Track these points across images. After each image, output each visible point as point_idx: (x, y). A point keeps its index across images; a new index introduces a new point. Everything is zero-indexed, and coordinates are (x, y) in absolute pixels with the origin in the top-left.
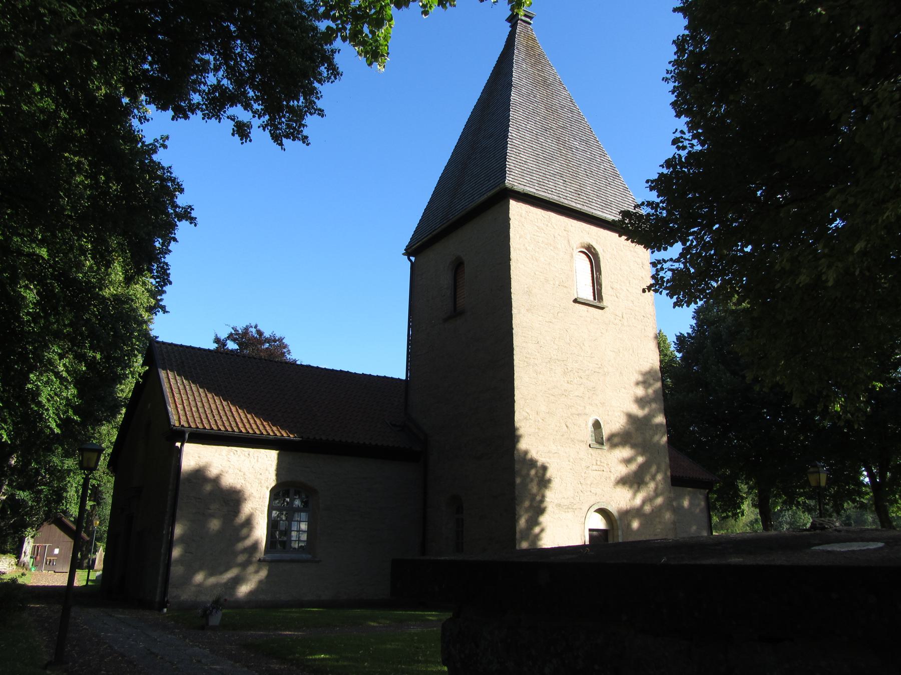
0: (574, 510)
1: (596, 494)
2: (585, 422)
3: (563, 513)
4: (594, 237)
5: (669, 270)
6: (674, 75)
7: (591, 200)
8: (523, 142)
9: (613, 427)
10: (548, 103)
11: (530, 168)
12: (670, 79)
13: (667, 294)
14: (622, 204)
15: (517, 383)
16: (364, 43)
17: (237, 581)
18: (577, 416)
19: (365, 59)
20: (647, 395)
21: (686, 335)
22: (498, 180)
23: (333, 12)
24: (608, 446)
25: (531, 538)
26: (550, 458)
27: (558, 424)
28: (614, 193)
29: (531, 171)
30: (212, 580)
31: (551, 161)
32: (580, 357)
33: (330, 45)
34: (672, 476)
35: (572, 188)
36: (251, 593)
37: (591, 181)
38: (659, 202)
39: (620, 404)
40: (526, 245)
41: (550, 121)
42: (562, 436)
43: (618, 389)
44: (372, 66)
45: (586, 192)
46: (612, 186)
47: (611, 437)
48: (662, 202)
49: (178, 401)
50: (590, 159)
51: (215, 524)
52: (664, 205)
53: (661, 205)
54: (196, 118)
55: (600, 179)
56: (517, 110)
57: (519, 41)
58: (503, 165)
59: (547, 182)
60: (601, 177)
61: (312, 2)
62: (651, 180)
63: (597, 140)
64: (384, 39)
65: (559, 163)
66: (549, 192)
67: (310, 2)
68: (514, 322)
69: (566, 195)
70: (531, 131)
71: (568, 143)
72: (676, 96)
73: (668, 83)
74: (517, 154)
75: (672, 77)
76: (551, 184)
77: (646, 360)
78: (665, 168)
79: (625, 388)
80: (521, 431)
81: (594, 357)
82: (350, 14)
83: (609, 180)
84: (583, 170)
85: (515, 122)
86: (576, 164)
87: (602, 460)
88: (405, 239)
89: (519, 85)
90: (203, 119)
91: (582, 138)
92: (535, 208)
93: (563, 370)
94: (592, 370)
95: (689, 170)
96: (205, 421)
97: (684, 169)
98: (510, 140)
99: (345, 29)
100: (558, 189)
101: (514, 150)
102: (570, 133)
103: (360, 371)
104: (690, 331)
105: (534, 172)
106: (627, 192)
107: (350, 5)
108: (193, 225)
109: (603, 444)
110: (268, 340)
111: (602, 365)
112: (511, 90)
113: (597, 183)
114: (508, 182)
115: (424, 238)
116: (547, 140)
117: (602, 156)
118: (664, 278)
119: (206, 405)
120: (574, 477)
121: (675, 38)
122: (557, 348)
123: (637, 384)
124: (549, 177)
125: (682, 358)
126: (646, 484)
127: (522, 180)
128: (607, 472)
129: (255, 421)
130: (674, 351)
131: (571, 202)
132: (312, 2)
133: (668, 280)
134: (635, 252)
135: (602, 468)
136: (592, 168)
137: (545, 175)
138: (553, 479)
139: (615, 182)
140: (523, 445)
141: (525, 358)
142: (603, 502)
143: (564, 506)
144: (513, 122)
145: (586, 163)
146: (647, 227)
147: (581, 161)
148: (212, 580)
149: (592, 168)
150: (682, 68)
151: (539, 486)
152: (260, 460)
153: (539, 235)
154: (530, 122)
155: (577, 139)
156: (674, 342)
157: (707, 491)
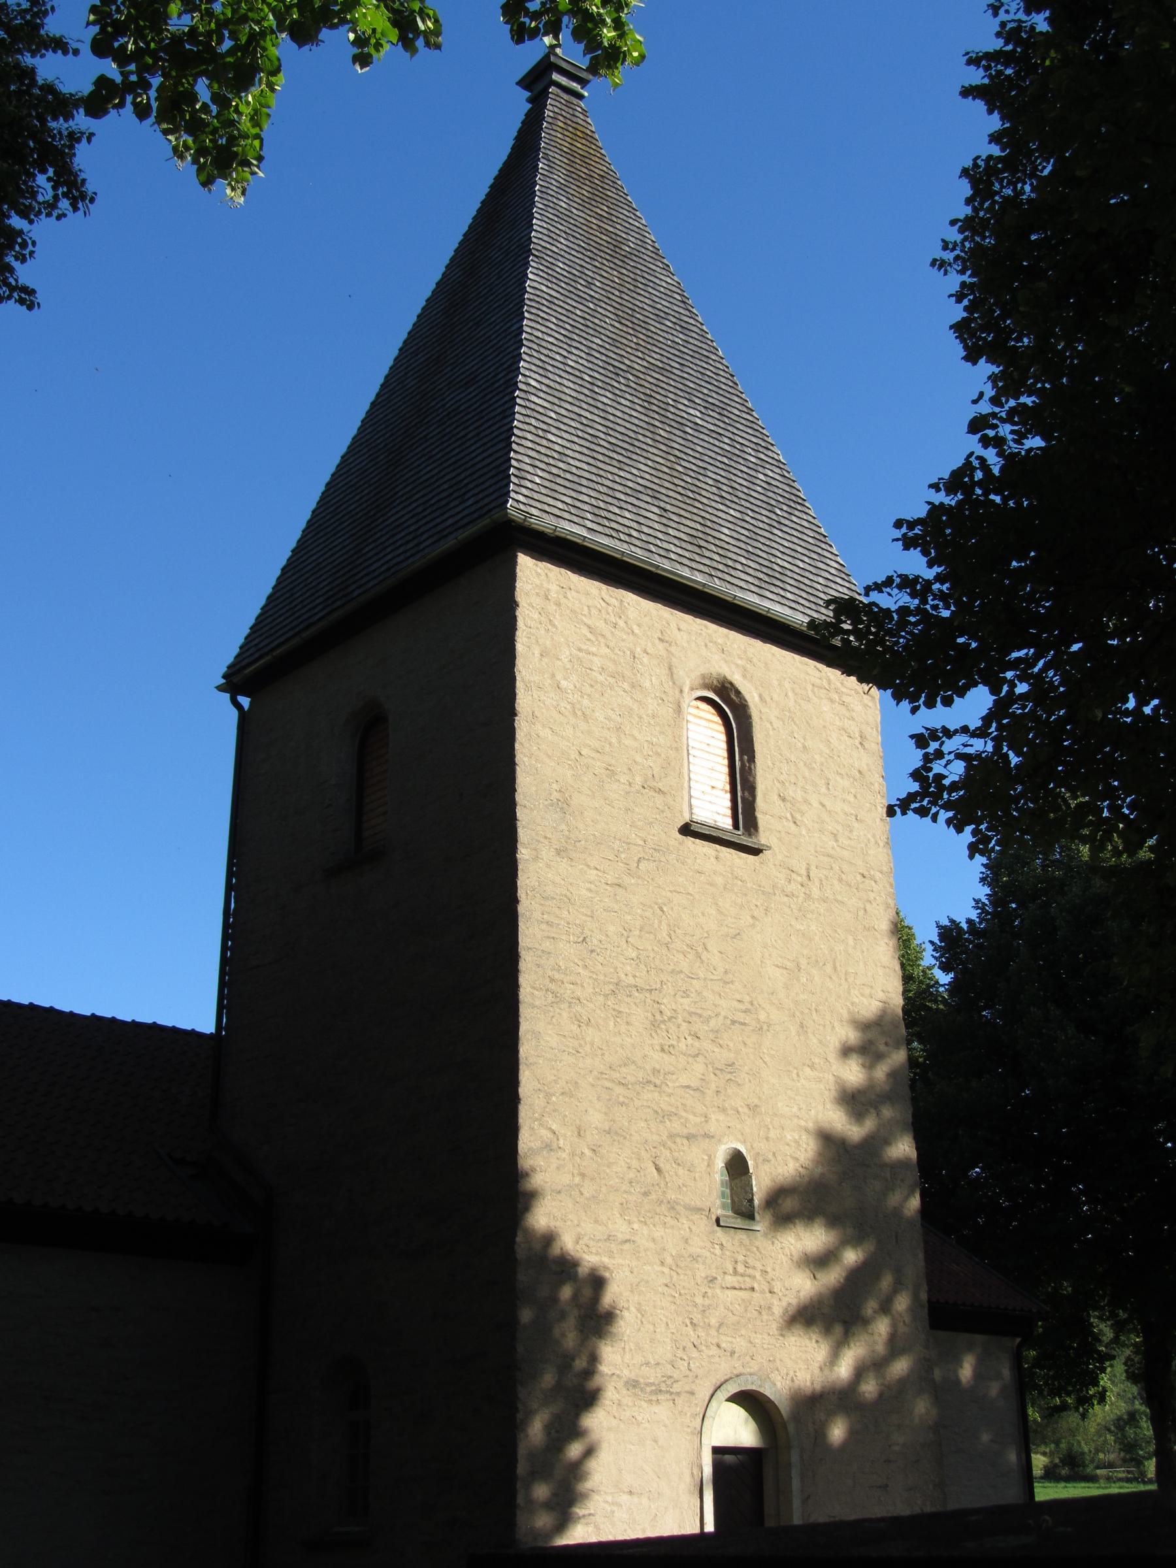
0: (674, 1396)
1: (733, 1353)
2: (706, 1158)
3: (644, 1404)
4: (740, 662)
5: (960, 756)
6: (963, 254)
7: (730, 563)
8: (556, 401)
9: (780, 1170)
10: (624, 303)
11: (574, 470)
12: (950, 265)
13: (949, 822)
14: (811, 577)
15: (526, 1050)
16: (195, 127)
18: (685, 1141)
19: (195, 167)
21: (965, 926)
22: (486, 501)
23: (123, 40)
24: (767, 1223)
26: (611, 1255)
27: (635, 1163)
28: (791, 545)
29: (576, 479)
31: (629, 454)
32: (694, 982)
33: (66, 120)
34: (929, 1301)
35: (682, 528)
37: (732, 512)
38: (931, 578)
39: (800, 1109)
40: (559, 677)
41: (629, 350)
42: (646, 1194)
43: (795, 1068)
44: (214, 188)
45: (717, 542)
46: (785, 529)
47: (775, 1198)
48: (939, 578)
50: (729, 455)
52: (945, 588)
53: (936, 586)
55: (756, 509)
56: (543, 318)
57: (551, 137)
58: (502, 460)
59: (617, 511)
60: (759, 503)
61: (26, 5)
62: (907, 521)
63: (750, 405)
64: (252, 119)
65: (650, 463)
66: (622, 537)
67: (19, 5)
69: (665, 545)
70: (577, 373)
71: (672, 410)
72: (966, 309)
73: (946, 273)
74: (540, 433)
75: (957, 258)
76: (627, 514)
77: (867, 991)
78: (943, 493)
79: (812, 1067)
80: (537, 1180)
81: (732, 982)
82: (165, 49)
83: (779, 512)
84: (710, 482)
85: (535, 347)
86: (694, 468)
87: (751, 1261)
89: (549, 253)
91: (710, 400)
92: (583, 578)
93: (650, 1015)
94: (725, 1018)
95: (1005, 500)
97: (992, 497)
98: (522, 395)
99: (147, 86)
100: (646, 530)
101: (533, 422)
102: (680, 386)
103: (84, 1009)
104: (974, 915)
105: (584, 482)
106: (823, 546)
107: (167, 24)
111: (752, 1004)
112: (527, 264)
113: (748, 519)
114: (515, 504)
115: (279, 646)
116: (620, 400)
117: (761, 449)
118: (945, 777)
120: (673, 1307)
121: (968, 163)
122: (634, 955)
123: (846, 1051)
124: (622, 497)
125: (954, 987)
126: (866, 1322)
127: (551, 501)
128: (763, 1292)
130: (930, 968)
131: (678, 566)
132: (26, 5)
133: (953, 783)
135: (748, 1282)
136: (734, 478)
137: (610, 493)
138: (618, 1312)
139: (794, 519)
140: (541, 1218)
141: (548, 980)
142: (751, 1374)
143: (647, 1385)
144: (530, 348)
145: (718, 464)
146: (897, 643)
147: (706, 458)
149: (734, 478)
150: (984, 238)
151: (582, 1331)
153: (594, 649)
154: (574, 351)
155: (697, 401)
156: (931, 942)
157: (1018, 1340)
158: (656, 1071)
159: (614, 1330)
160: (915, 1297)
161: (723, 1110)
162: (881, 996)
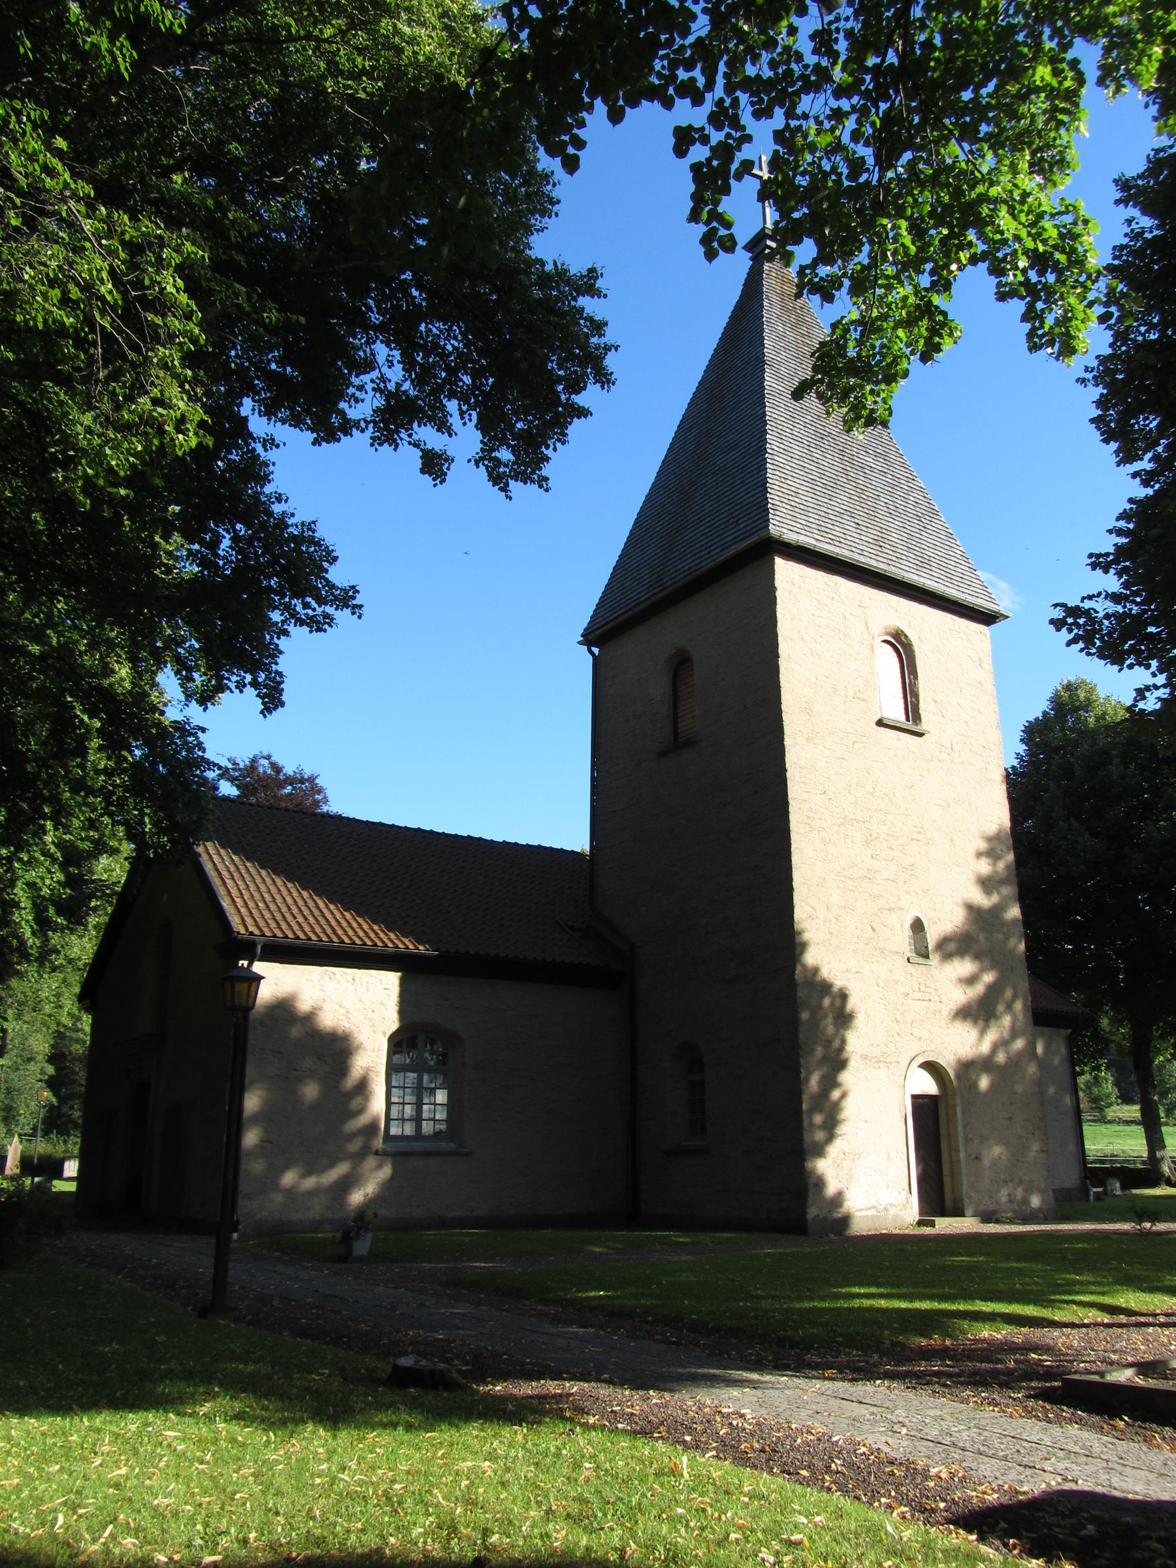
15: (795, 859)
17: (346, 1185)
20: (996, 872)
25: (827, 1106)
27: (860, 926)
30: (310, 1182)
36: (370, 1203)
42: (867, 944)
47: (942, 944)
49: (234, 892)
51: (311, 1091)
77: (989, 818)
80: (806, 936)
87: (929, 984)
88: (583, 618)
90: (372, 445)
96: (284, 926)
108: (355, 616)
109: (927, 957)
110: (290, 780)
112: (763, 371)
119: (279, 900)
123: (979, 855)
129: (359, 924)
134: (968, 640)
135: (928, 996)
140: (811, 957)
148: (310, 1182)
152: (371, 988)
158: (869, 870)
159: (356, 1043)
160: (1025, 1005)
161: (908, 893)
162: (998, 821)
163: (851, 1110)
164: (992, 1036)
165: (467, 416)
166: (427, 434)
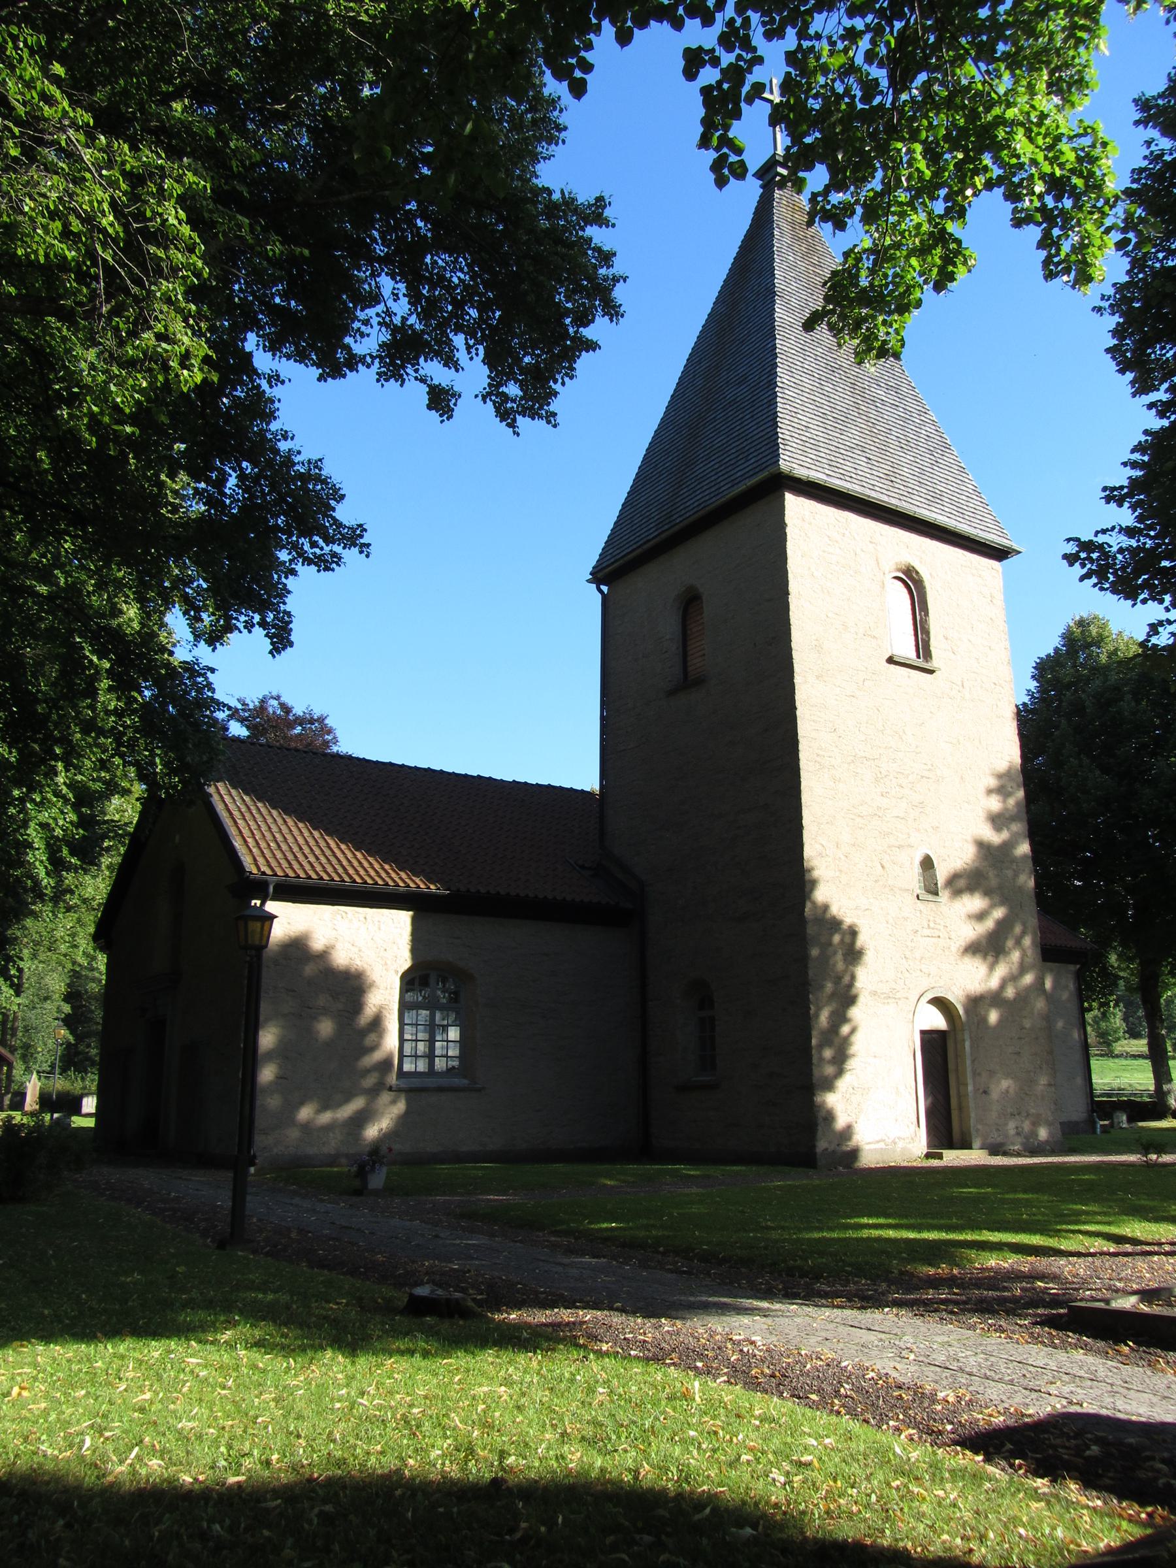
20: (1006, 809)
25: (837, 1041)
30: (326, 1117)
36: (386, 1137)
47: (952, 881)
49: (246, 832)
51: (326, 1028)
54: (365, 376)
68: (798, 697)
80: (816, 874)
103: (509, 778)
108: (363, 555)
109: (937, 894)
110: (300, 721)
123: (990, 792)
129: (370, 864)
135: (937, 933)
140: (821, 895)
148: (326, 1117)
158: (879, 808)
161: (918, 830)
163: (860, 1045)
164: (1001, 971)
165: (473, 351)
166: (434, 370)
